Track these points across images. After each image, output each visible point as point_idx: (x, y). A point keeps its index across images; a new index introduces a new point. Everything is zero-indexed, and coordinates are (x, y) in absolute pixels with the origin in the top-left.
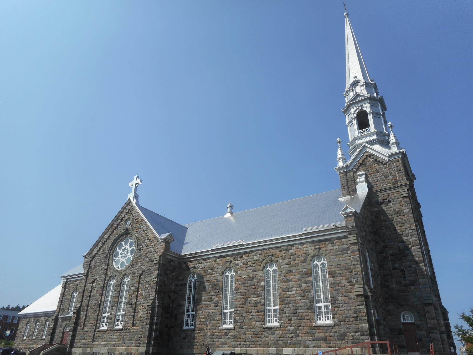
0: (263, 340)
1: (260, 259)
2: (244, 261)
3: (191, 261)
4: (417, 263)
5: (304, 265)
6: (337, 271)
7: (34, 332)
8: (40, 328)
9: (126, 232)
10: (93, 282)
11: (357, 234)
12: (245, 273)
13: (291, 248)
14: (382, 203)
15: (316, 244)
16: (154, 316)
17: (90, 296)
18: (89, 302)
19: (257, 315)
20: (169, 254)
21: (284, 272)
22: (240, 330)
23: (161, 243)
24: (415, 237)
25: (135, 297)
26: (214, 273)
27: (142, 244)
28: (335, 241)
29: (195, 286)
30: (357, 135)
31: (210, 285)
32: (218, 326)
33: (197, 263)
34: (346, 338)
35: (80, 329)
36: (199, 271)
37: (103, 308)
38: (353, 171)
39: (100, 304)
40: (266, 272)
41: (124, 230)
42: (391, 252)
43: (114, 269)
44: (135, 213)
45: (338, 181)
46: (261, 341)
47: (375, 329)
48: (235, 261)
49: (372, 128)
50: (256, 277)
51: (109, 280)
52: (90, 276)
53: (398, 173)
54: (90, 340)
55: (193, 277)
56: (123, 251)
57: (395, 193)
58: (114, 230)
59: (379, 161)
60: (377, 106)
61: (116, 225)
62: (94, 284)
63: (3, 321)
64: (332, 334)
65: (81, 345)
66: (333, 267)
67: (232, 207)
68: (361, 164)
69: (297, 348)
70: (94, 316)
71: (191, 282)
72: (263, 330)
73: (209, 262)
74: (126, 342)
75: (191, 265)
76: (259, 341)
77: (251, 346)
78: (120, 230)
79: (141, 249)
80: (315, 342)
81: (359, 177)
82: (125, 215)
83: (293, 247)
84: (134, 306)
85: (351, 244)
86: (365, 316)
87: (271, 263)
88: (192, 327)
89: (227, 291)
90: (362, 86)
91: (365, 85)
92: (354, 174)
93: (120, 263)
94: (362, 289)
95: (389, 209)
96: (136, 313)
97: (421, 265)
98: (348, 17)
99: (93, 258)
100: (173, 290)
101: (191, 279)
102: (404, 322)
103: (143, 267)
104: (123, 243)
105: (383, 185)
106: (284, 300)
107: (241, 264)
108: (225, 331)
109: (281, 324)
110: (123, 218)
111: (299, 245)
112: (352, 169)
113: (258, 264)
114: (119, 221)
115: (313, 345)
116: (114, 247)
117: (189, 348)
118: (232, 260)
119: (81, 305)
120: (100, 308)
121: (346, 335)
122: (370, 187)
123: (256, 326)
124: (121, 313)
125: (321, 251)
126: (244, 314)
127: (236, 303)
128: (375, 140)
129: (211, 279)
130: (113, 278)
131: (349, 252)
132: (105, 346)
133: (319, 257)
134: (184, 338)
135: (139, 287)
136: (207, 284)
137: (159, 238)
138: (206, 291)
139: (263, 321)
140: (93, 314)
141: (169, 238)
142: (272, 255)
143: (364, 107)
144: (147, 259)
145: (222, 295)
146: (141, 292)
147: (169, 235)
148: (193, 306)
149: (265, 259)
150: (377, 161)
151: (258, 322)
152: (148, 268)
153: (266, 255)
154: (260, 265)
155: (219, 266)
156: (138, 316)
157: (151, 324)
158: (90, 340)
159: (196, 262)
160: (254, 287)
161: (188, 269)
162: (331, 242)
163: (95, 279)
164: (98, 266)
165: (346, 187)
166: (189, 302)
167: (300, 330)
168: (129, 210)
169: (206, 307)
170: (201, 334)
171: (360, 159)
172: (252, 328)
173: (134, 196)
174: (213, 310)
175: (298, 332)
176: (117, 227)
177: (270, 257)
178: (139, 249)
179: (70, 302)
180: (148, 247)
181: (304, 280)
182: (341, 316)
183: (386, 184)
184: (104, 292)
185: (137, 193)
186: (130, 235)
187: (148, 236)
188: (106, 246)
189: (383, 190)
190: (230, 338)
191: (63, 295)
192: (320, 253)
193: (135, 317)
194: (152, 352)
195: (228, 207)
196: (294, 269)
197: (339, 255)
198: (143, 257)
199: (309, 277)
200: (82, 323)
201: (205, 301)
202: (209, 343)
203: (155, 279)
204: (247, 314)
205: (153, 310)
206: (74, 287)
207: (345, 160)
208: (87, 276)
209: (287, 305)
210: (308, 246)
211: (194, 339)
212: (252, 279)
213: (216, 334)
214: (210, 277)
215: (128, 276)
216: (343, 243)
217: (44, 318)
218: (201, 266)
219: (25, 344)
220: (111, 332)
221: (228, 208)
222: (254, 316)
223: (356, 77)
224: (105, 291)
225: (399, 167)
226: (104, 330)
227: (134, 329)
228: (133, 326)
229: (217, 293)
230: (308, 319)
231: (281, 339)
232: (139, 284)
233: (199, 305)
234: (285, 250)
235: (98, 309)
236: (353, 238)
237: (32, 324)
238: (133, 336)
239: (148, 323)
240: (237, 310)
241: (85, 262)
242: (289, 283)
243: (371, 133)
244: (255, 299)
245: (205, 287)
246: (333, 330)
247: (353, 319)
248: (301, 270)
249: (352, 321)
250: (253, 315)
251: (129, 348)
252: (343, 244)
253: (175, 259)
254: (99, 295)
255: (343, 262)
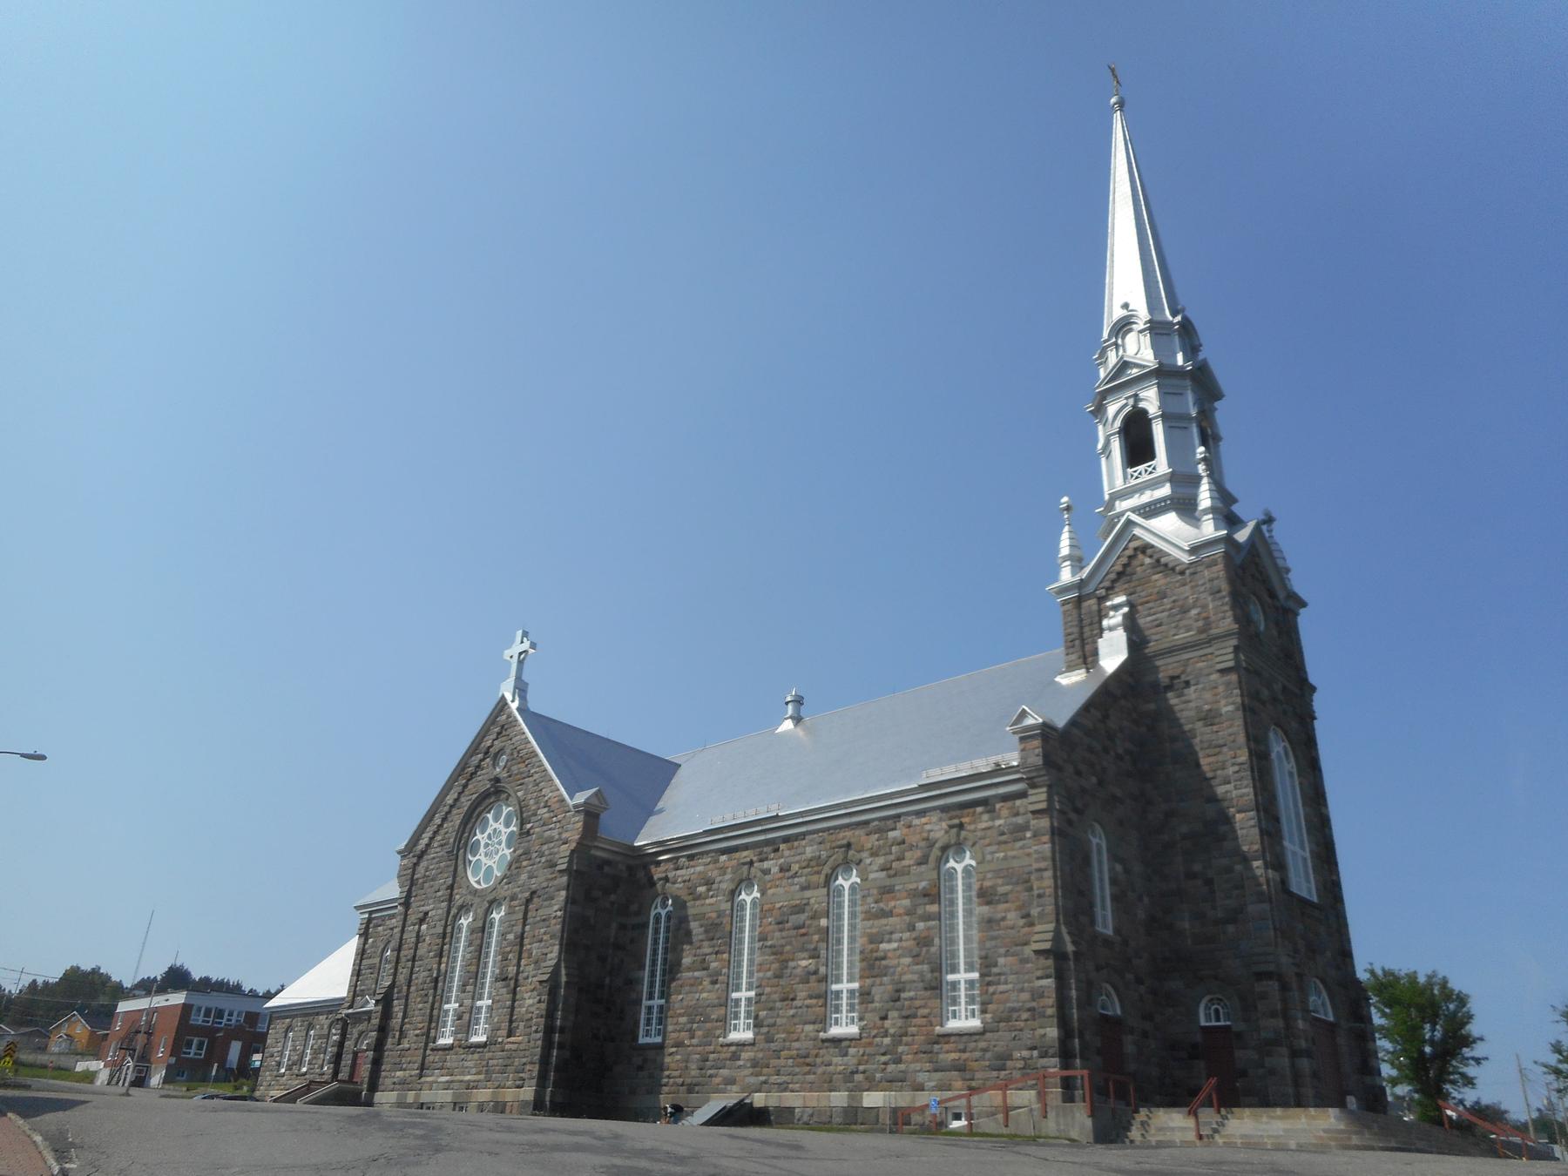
0: (820, 1070)
1: (820, 857)
2: (782, 860)
3: (658, 863)
4: (1245, 860)
5: (923, 870)
6: (999, 889)
7: (303, 1054)
8: (316, 1044)
9: (496, 788)
10: (421, 921)
11: (1050, 787)
12: (785, 894)
13: (893, 826)
14: (1170, 688)
15: (954, 813)
16: (556, 1009)
17: (414, 956)
18: (412, 973)
19: (808, 1007)
20: (596, 844)
21: (875, 891)
22: (767, 1046)
23: (574, 816)
24: (1246, 787)
25: (515, 962)
26: (711, 893)
27: (533, 819)
28: (998, 806)
29: (667, 929)
30: (1119, 484)
31: (701, 926)
32: (717, 1035)
33: (672, 866)
34: (1009, 1063)
35: (393, 1044)
36: (677, 888)
37: (443, 990)
38: (1099, 596)
39: (437, 979)
40: (945, 875)
41: (490, 780)
42: (1184, 829)
43: (469, 886)
44: (516, 735)
45: (1055, 624)
46: (814, 1073)
47: (1077, 1040)
48: (761, 861)
49: (1161, 463)
50: (807, 904)
51: (458, 917)
52: (413, 905)
53: (1213, 600)
54: (414, 1073)
55: (664, 905)
56: (489, 837)
57: (1203, 658)
58: (469, 780)
59: (1166, 565)
60: (1180, 392)
61: (471, 769)
62: (424, 927)
63: (247, 1029)
64: (978, 1054)
65: (394, 1083)
66: (989, 875)
67: (798, 701)
68: (1120, 575)
69: (896, 1091)
70: (423, 1011)
71: (658, 918)
72: (820, 1043)
73: (699, 865)
74: (494, 1075)
75: (657, 873)
76: (809, 1073)
77: (791, 1086)
78: (481, 783)
79: (528, 833)
80: (938, 1075)
81: (1112, 613)
82: (494, 740)
83: (899, 821)
84: (511, 983)
85: (1033, 812)
86: (1052, 1006)
87: (846, 865)
88: (659, 1040)
89: (741, 941)
90: (1140, 332)
91: (1150, 329)
92: (1099, 604)
93: (483, 870)
94: (1050, 936)
95: (1187, 705)
96: (516, 1003)
97: (1256, 864)
98: (1121, 110)
99: (420, 856)
100: (612, 940)
101: (659, 910)
102: (1207, 1024)
103: (533, 881)
104: (490, 816)
105: (1174, 635)
106: (872, 965)
107: (775, 870)
108: (733, 1048)
109: (863, 1029)
110: (489, 747)
111: (914, 817)
112: (1096, 590)
113: (815, 869)
114: (480, 756)
115: (933, 1084)
116: (470, 826)
117: (649, 1092)
118: (755, 859)
119: (394, 982)
120: (435, 988)
121: (1010, 1057)
122: (1137, 642)
123: (804, 1034)
124: (744, 994)
125: (963, 833)
126: (778, 1005)
127: (761, 975)
128: (1164, 499)
129: (703, 910)
130: (468, 911)
131: (1028, 834)
132: (447, 1086)
133: (958, 848)
134: (640, 1068)
135: (525, 935)
136: (694, 925)
137: (571, 803)
138: (691, 943)
139: (823, 1022)
140: (420, 1006)
141: (595, 801)
142: (849, 846)
143: (1142, 400)
144: (543, 859)
145: (730, 953)
146: (529, 947)
147: (596, 794)
148: (663, 983)
149: (830, 857)
150: (1162, 564)
151: (810, 1023)
152: (545, 885)
153: (834, 845)
154: (819, 873)
155: (725, 874)
156: (521, 1011)
157: (549, 1030)
158: (414, 1073)
159: (671, 866)
160: (803, 931)
161: (652, 884)
162: (989, 807)
163: (426, 914)
164: (433, 880)
165: (1077, 642)
166: (653, 974)
167: (906, 1045)
168: (503, 727)
169: (692, 985)
170: (679, 1057)
171: (1118, 558)
172: (795, 1041)
173: (515, 687)
174: (707, 995)
175: (900, 1049)
176: (475, 773)
177: (843, 849)
178: (524, 833)
179: (378, 975)
180: (545, 828)
181: (920, 911)
182: (1001, 1007)
183: (1182, 631)
184: (446, 947)
185: (525, 677)
186: (504, 796)
187: (546, 798)
188: (450, 824)
189: (1171, 651)
190: (744, 1067)
191: (363, 955)
192: (961, 838)
193: (515, 1013)
194: (551, 1101)
195: (790, 702)
196: (899, 884)
197: (1006, 842)
198: (535, 855)
199: (932, 903)
200: (398, 1028)
201: (689, 969)
202: (695, 1080)
203: (559, 913)
204: (786, 1003)
205: (553, 993)
206: (386, 933)
207: (1077, 562)
208: (406, 904)
209: (878, 980)
210: (934, 819)
211: (662, 1070)
212: (799, 909)
213: (712, 1056)
214: (703, 905)
215: (500, 905)
216: (1015, 811)
217: (325, 1016)
218: (682, 876)
219: (282, 1087)
220: (462, 1051)
221: (787, 703)
222: (800, 1007)
223: (1126, 306)
224: (448, 946)
225: (1216, 582)
226: (446, 1045)
227: (510, 1043)
228: (509, 1035)
229: (717, 949)
230: (924, 1017)
231: (861, 1068)
232: (524, 925)
233: (673, 979)
234: (880, 831)
235: (431, 991)
236: (1039, 798)
237: (299, 1034)
238: (509, 1062)
239: (542, 1027)
240: (763, 994)
241: (403, 868)
242: (884, 921)
243: (1143, 485)
244: (804, 963)
245: (689, 933)
246: (982, 1044)
247: (1029, 1013)
248: (913, 886)
249: (1026, 1020)
250: (799, 1005)
251: (499, 1093)
252: (1017, 814)
253: (618, 858)
254: (435, 957)
255: (1015, 863)
